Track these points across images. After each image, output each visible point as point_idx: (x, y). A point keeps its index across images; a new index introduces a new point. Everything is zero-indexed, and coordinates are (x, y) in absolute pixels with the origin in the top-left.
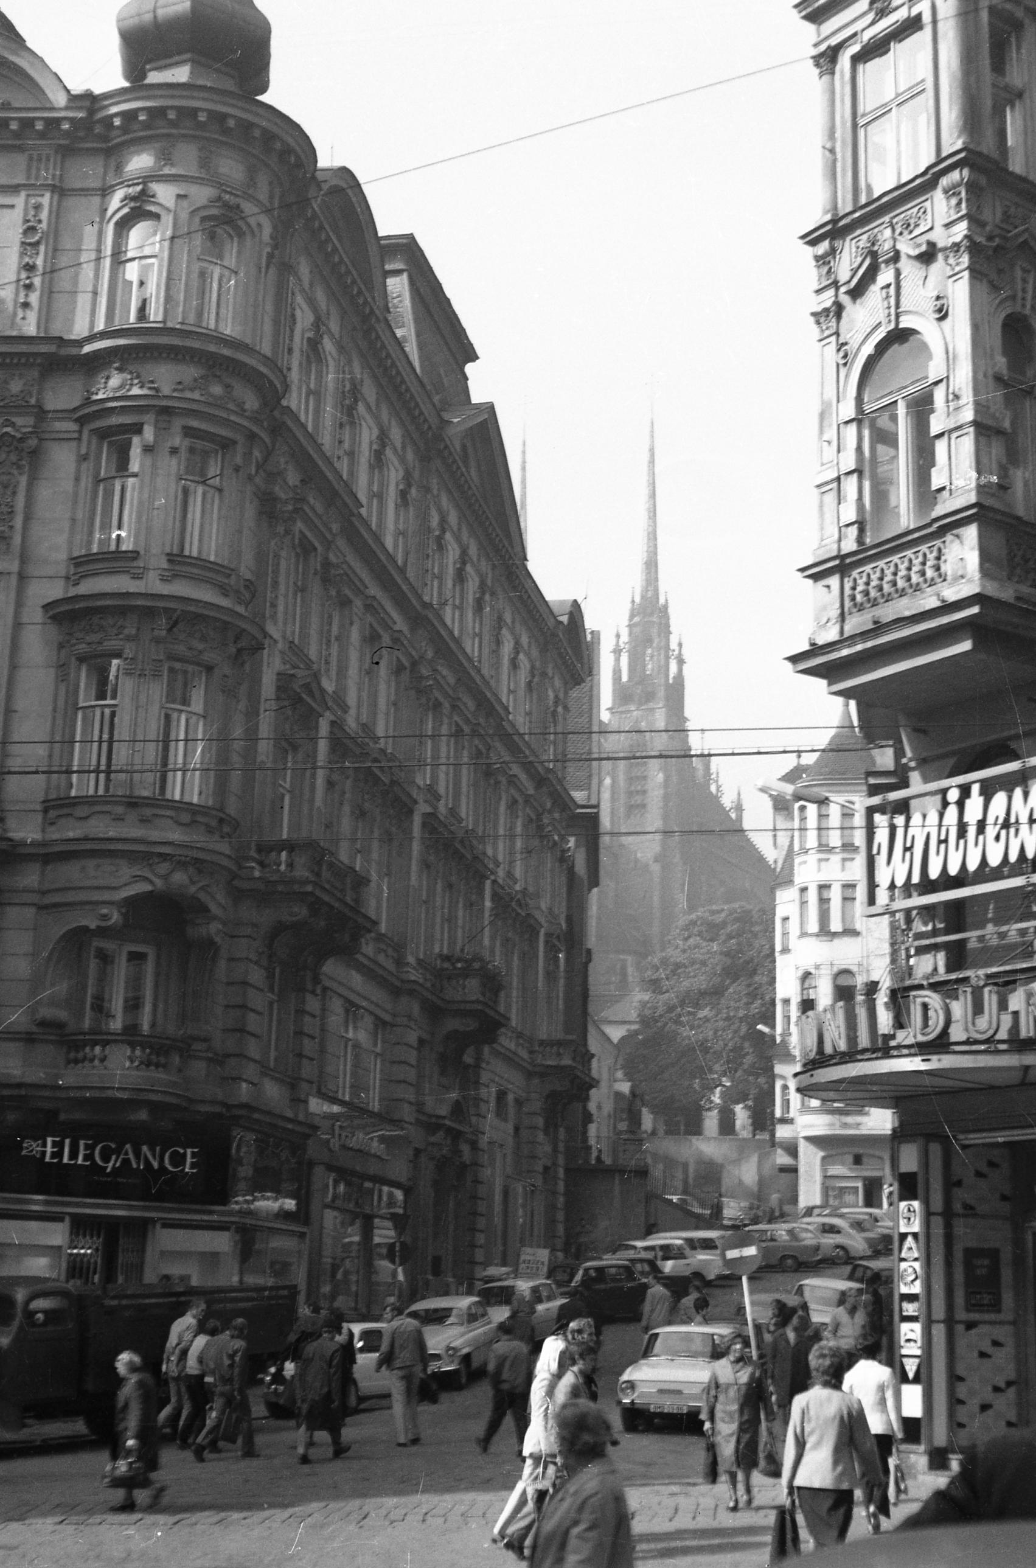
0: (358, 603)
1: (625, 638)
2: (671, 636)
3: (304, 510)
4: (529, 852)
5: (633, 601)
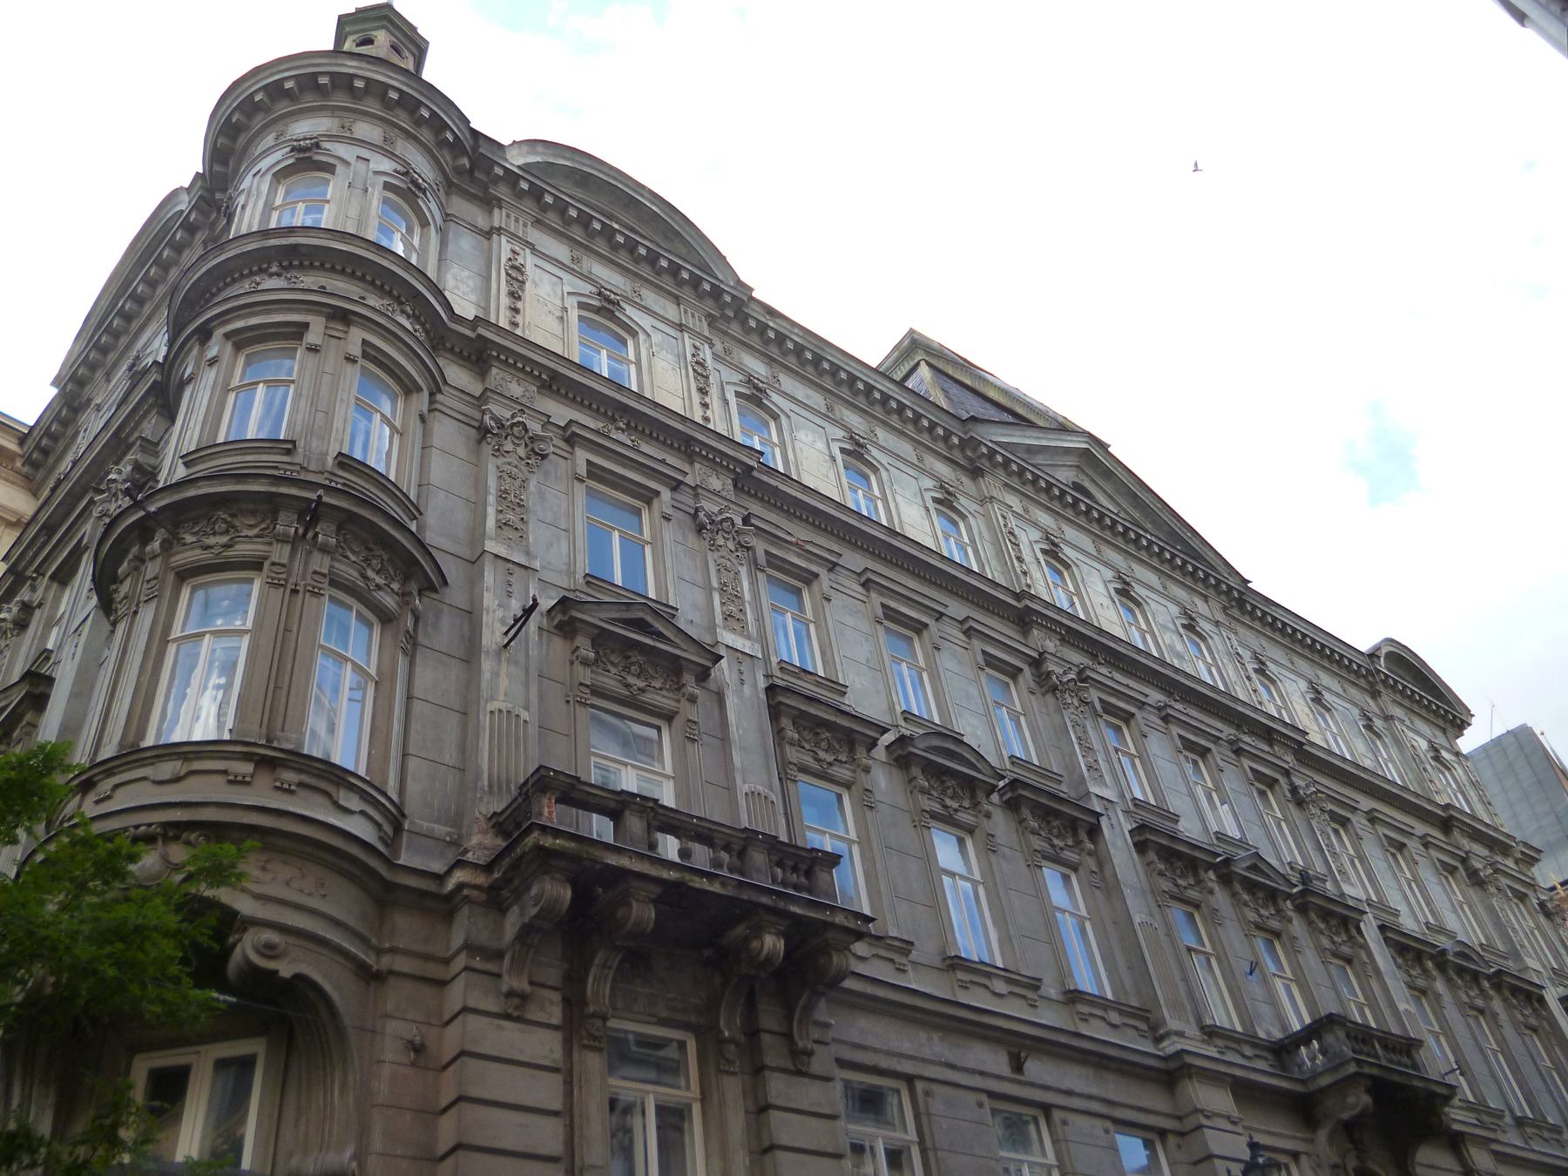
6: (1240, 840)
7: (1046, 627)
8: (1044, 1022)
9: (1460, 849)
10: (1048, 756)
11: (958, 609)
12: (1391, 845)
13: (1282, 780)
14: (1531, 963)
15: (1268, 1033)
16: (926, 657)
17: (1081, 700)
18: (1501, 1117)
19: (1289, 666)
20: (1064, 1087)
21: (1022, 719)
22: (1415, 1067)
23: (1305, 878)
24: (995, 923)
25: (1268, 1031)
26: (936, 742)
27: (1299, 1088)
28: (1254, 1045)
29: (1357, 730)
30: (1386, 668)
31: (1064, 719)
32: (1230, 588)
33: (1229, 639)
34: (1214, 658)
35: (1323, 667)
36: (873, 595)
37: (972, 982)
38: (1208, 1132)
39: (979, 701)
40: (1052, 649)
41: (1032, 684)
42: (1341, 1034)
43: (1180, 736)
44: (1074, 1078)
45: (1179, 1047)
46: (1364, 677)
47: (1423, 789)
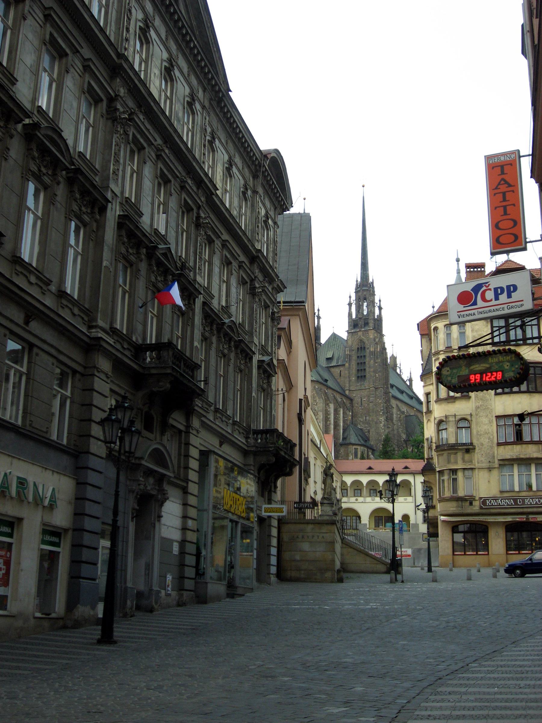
0: (235, 264)
1: (353, 298)
2: (376, 296)
3: (243, 266)
4: (198, 658)
5: (357, 281)
6: (163, 236)
7: (125, 79)
8: (46, 303)
9: (253, 274)
10: (96, 156)
11: (87, 53)
12: (185, 206)
13: (195, 210)
14: (256, 340)
15: (137, 339)
16: (59, 74)
17: (124, 131)
18: (210, 406)
19: (225, 144)
20: (43, 338)
21: (91, 129)
22: (192, 377)
23: (184, 266)
24: (40, 242)
25: (136, 338)
26: (50, 133)
27: (141, 370)
28: (129, 344)
29: (238, 193)
30: (269, 166)
31: (112, 139)
32: (220, 90)
33: (205, 119)
34: (193, 127)
35: (240, 152)
36: (87, 75)
37: (22, 273)
38: (96, 379)
39: (76, 112)
40: (122, 94)
41: (104, 112)
42: (171, 353)
43: (161, 169)
44: (48, 335)
45: (100, 335)
46: (256, 165)
47: (252, 236)
